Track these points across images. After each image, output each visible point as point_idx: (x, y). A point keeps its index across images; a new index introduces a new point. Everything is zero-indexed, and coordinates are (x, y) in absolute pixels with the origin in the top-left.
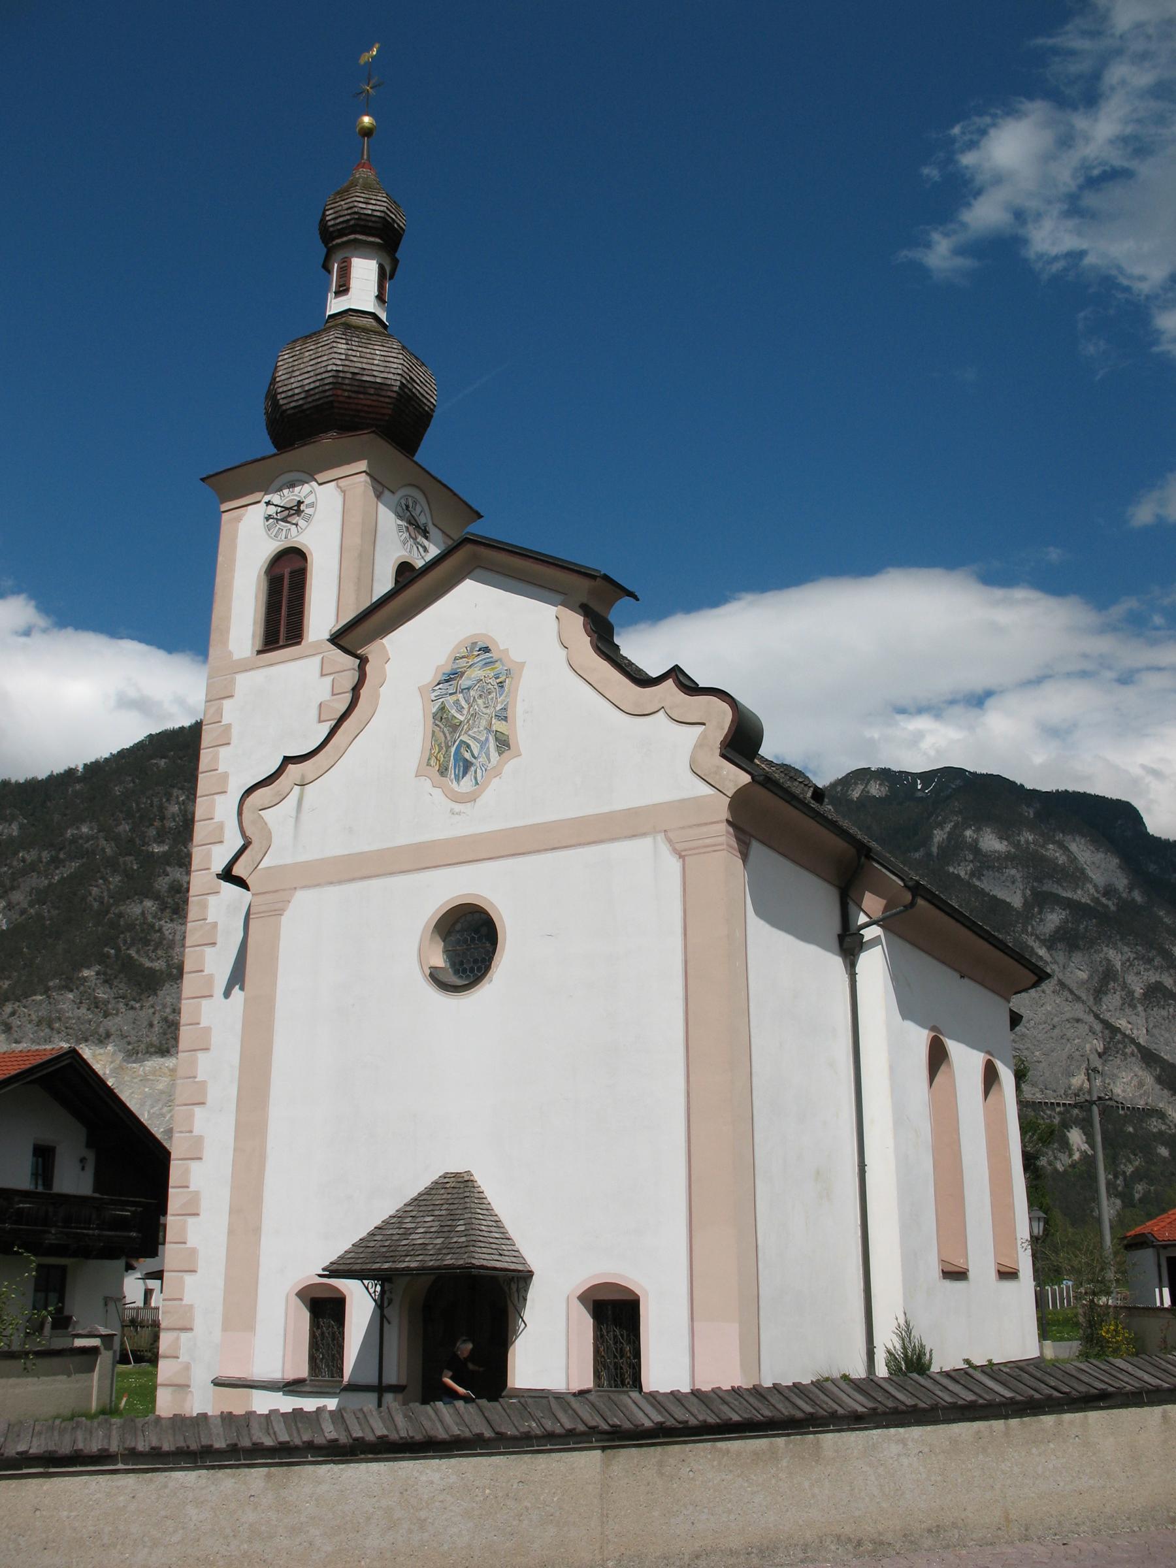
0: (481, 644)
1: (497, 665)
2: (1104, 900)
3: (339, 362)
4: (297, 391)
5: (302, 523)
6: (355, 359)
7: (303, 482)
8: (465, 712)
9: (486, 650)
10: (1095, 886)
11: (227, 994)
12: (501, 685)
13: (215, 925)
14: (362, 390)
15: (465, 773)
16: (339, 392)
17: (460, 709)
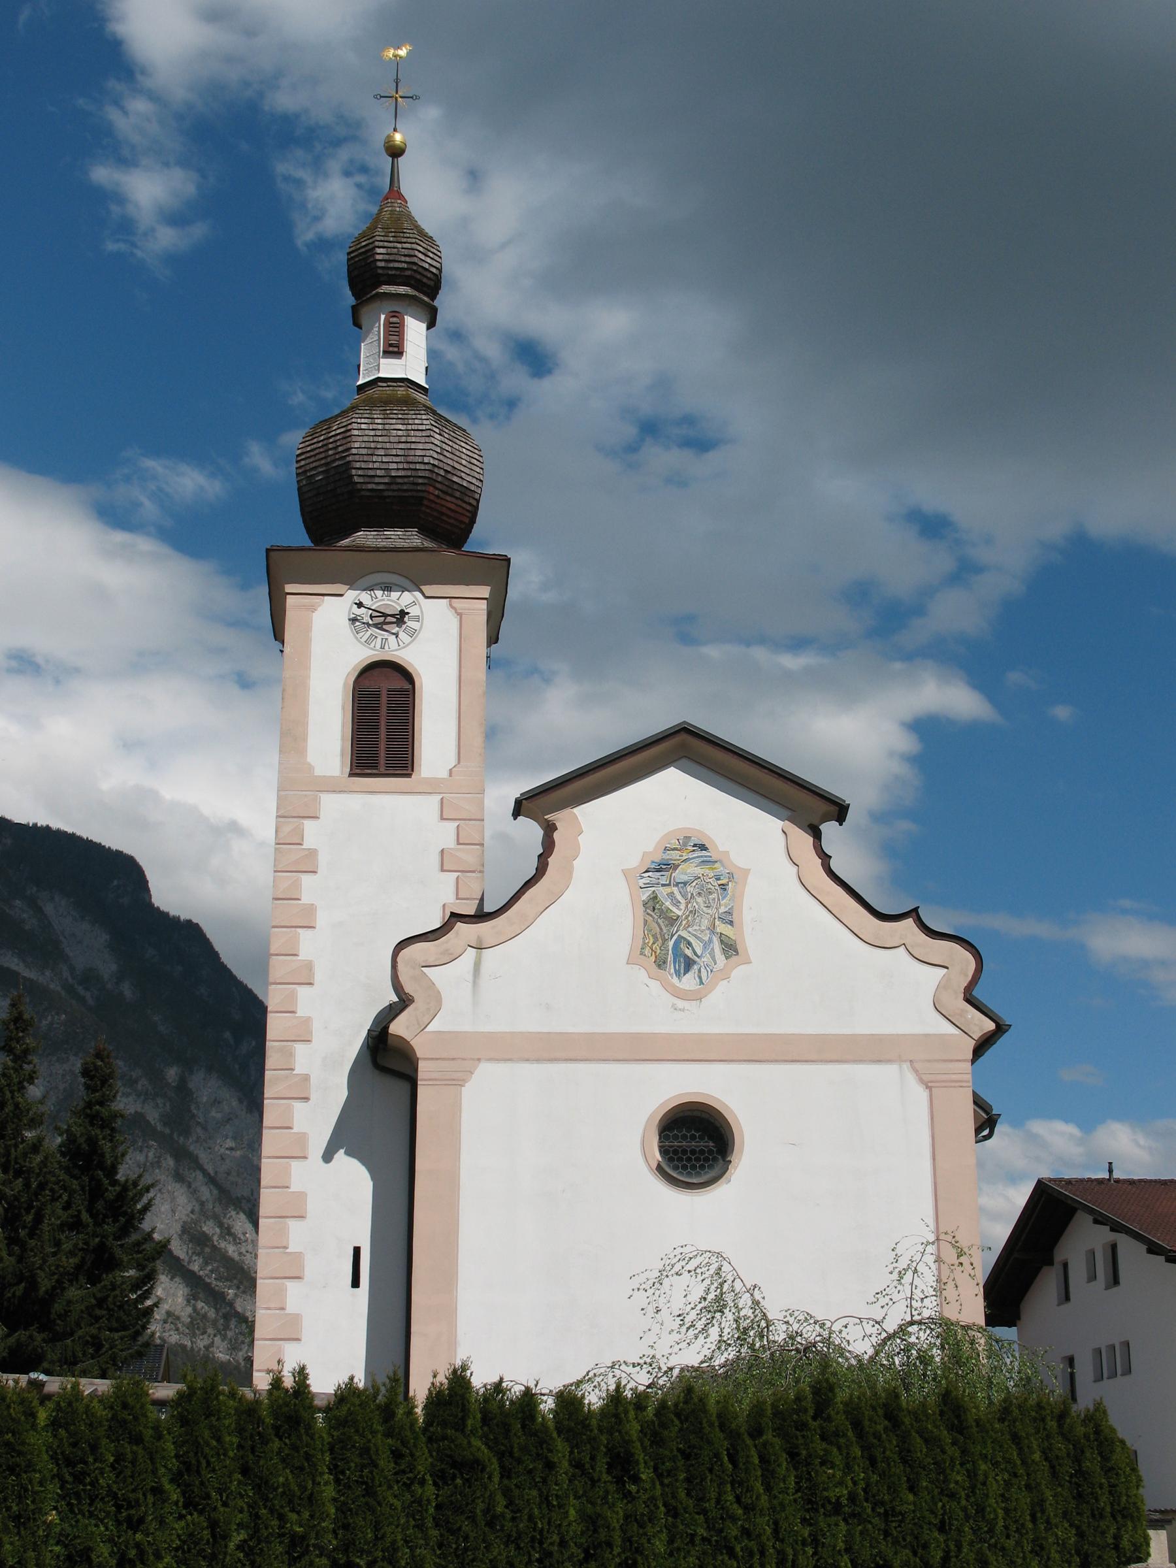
0: (695, 840)
1: (716, 865)
2: (80, 990)
3: (435, 455)
4: (379, 473)
5: (402, 635)
6: (447, 454)
7: (404, 589)
8: (683, 907)
9: (703, 847)
10: (72, 969)
11: (328, 1157)
12: (723, 887)
13: (306, 1078)
14: (450, 491)
15: (687, 970)
16: (431, 489)
17: (677, 903)
